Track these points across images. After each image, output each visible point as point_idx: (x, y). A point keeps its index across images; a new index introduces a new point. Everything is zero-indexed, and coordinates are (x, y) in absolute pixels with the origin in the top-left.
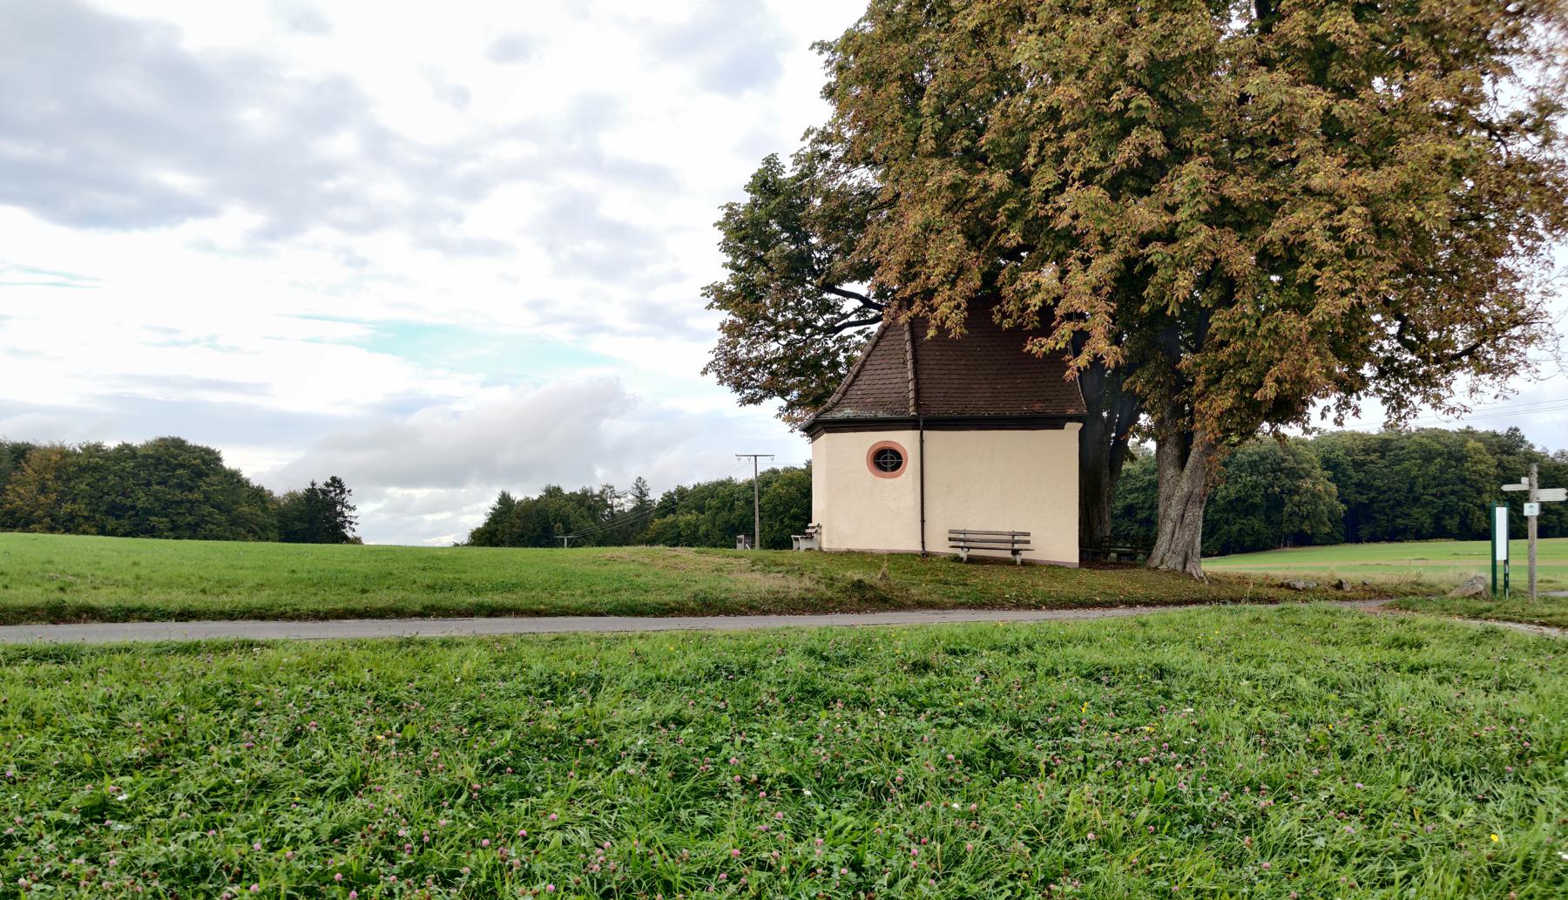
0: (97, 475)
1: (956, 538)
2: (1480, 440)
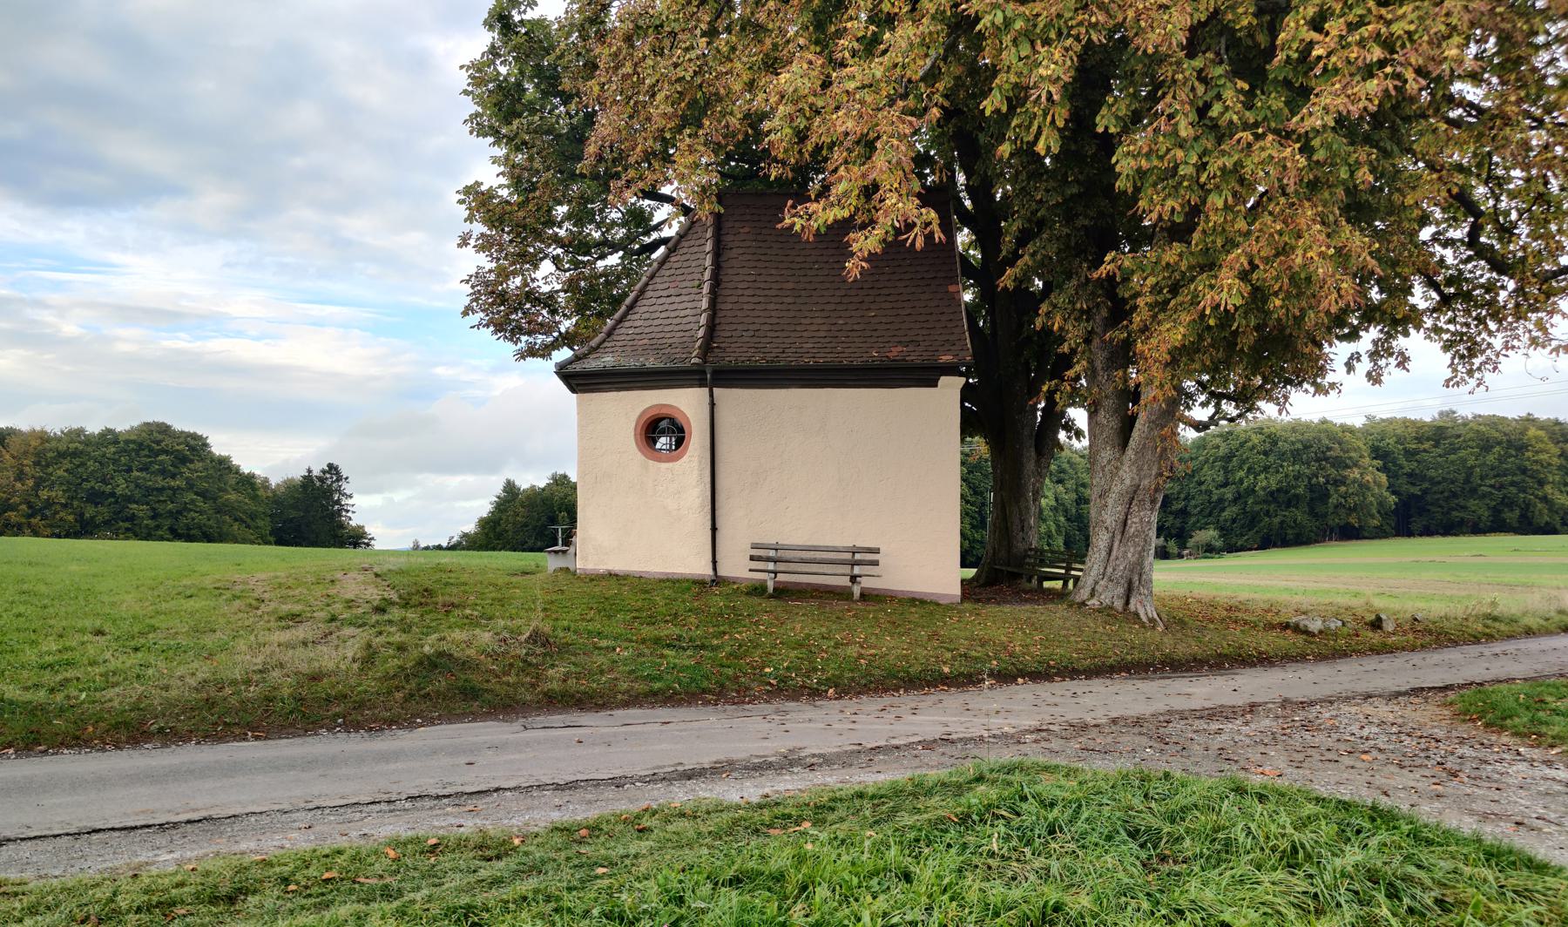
0: (77, 461)
2: (1542, 428)
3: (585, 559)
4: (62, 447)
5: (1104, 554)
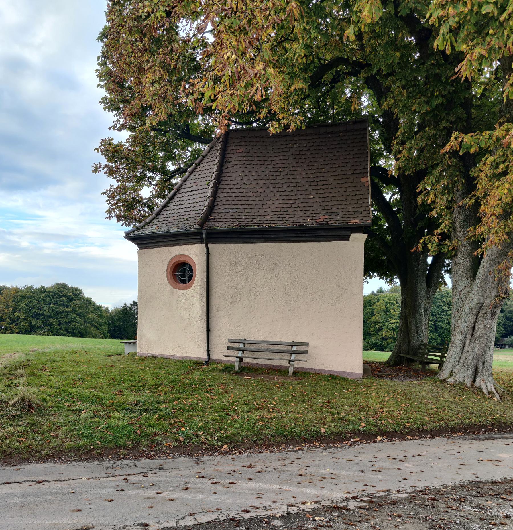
0: (29, 300)
1: (236, 345)
3: (141, 347)
4: (24, 294)
5: (459, 348)
